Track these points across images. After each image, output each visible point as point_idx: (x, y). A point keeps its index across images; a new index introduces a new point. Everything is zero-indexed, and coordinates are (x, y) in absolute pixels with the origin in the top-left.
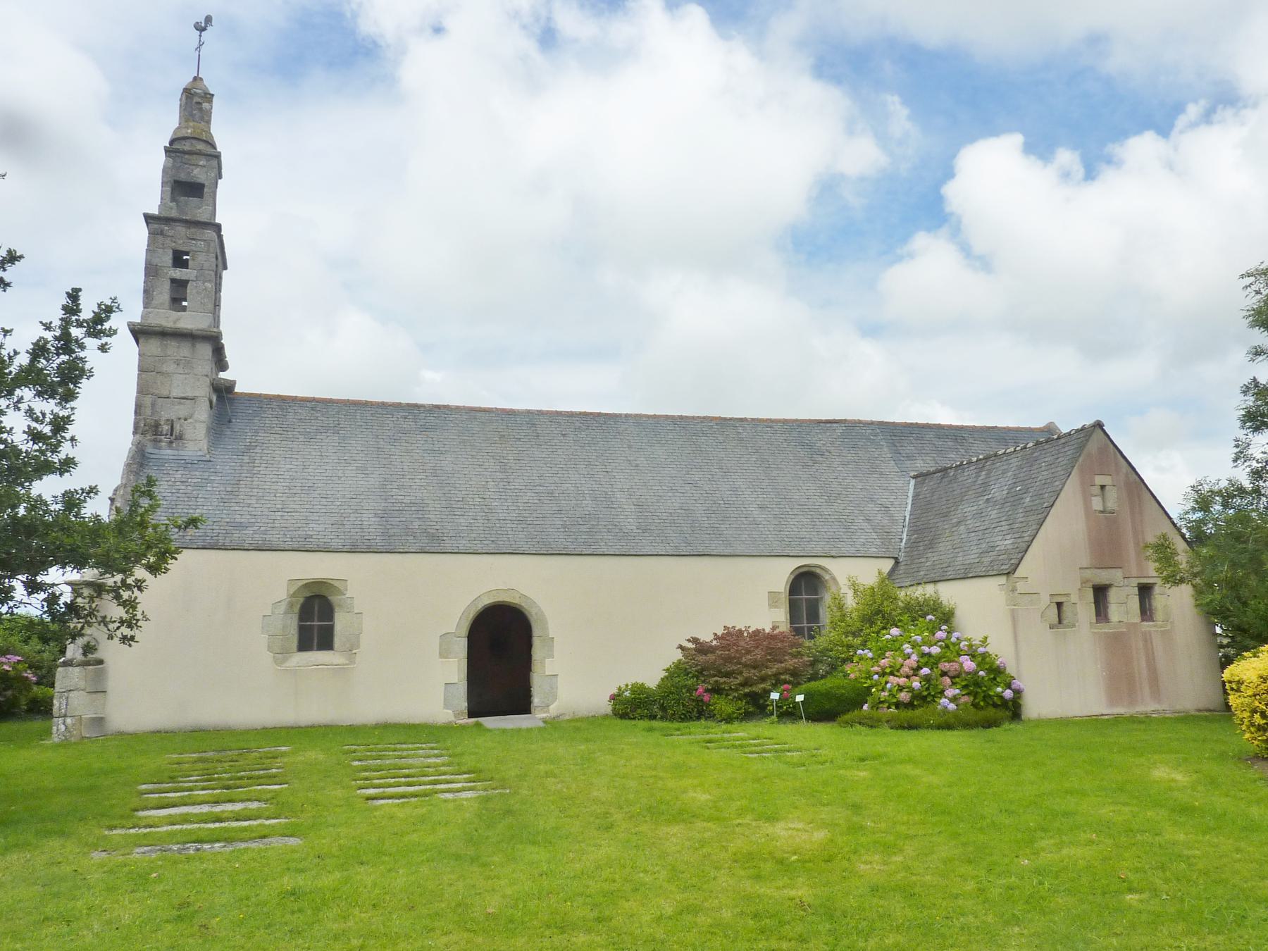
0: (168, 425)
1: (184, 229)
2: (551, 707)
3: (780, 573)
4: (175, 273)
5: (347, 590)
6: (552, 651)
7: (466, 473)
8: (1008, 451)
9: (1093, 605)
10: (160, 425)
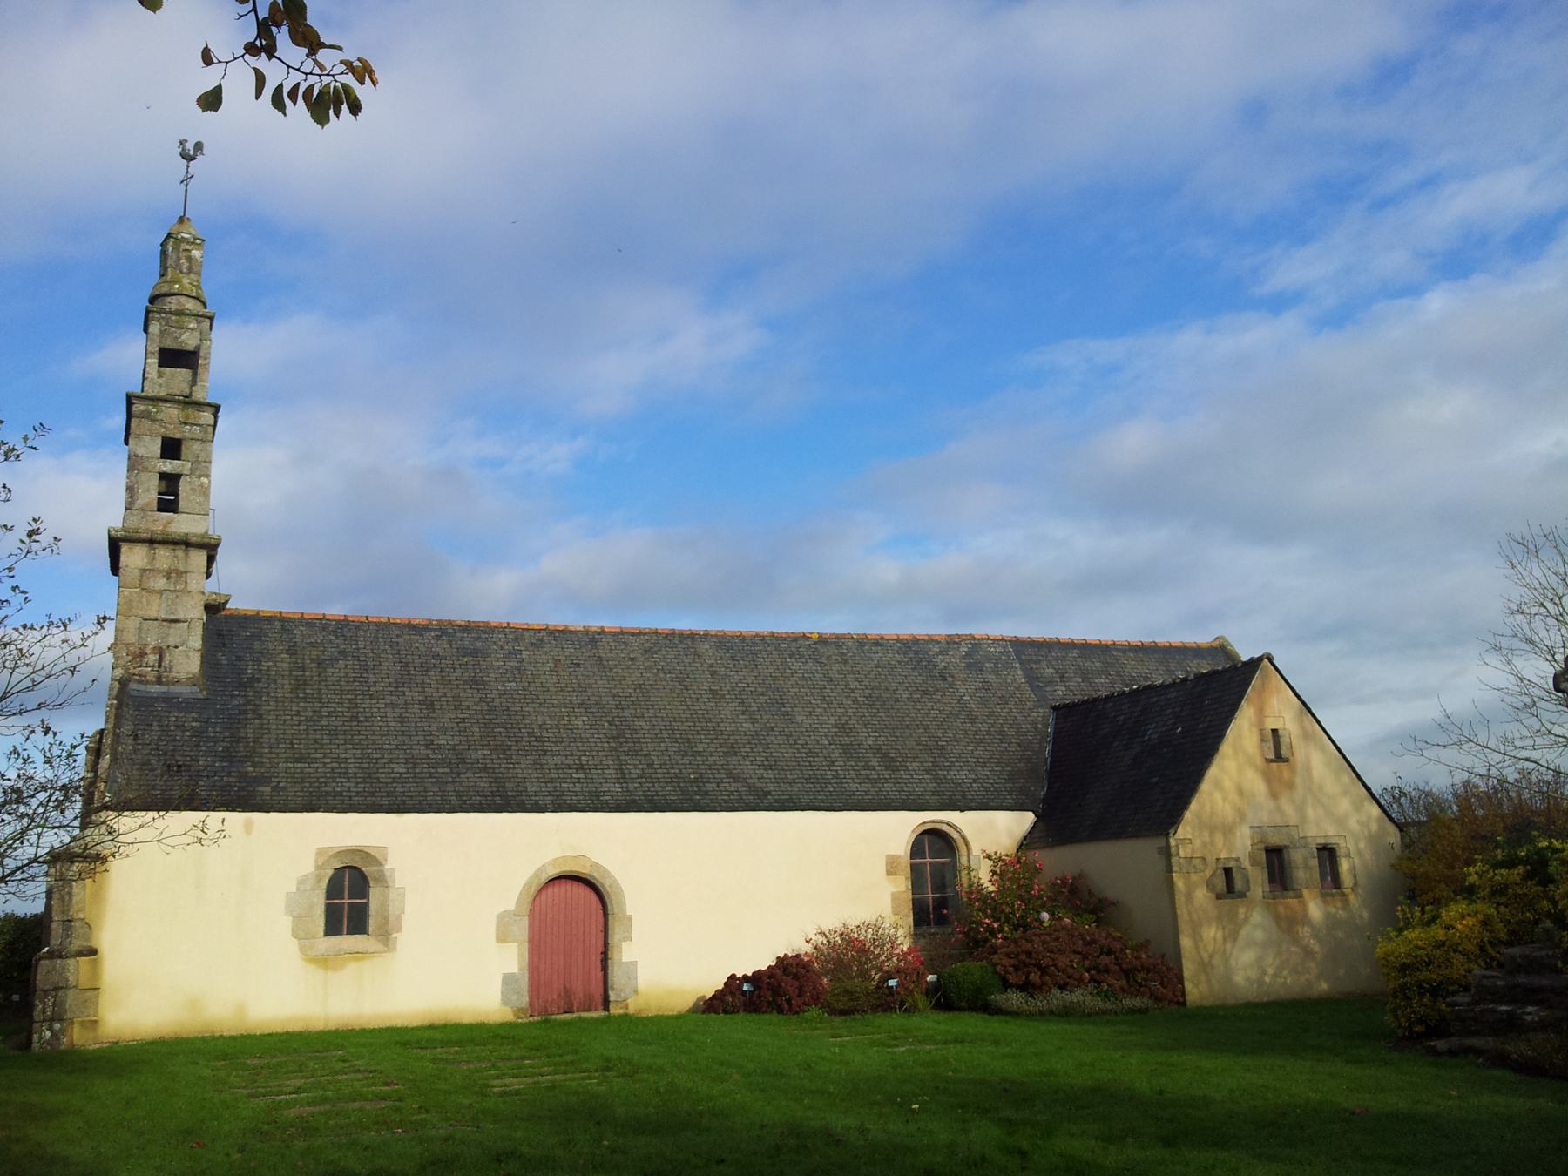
1: (176, 411)
4: (165, 466)
5: (386, 860)
6: (630, 932)
7: (594, 710)
10: (146, 654)
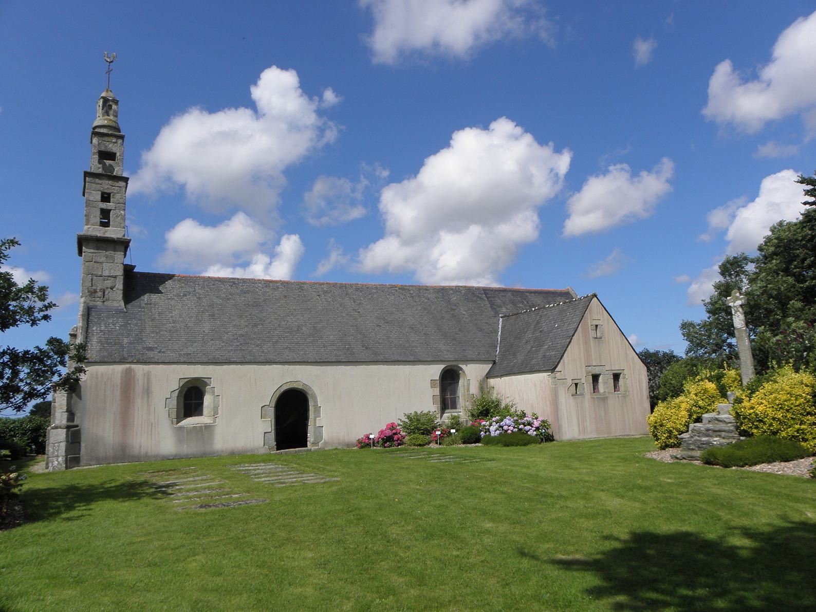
0: (101, 292)
2: (320, 443)
3: (436, 371)
8: (550, 306)
9: (612, 380)
